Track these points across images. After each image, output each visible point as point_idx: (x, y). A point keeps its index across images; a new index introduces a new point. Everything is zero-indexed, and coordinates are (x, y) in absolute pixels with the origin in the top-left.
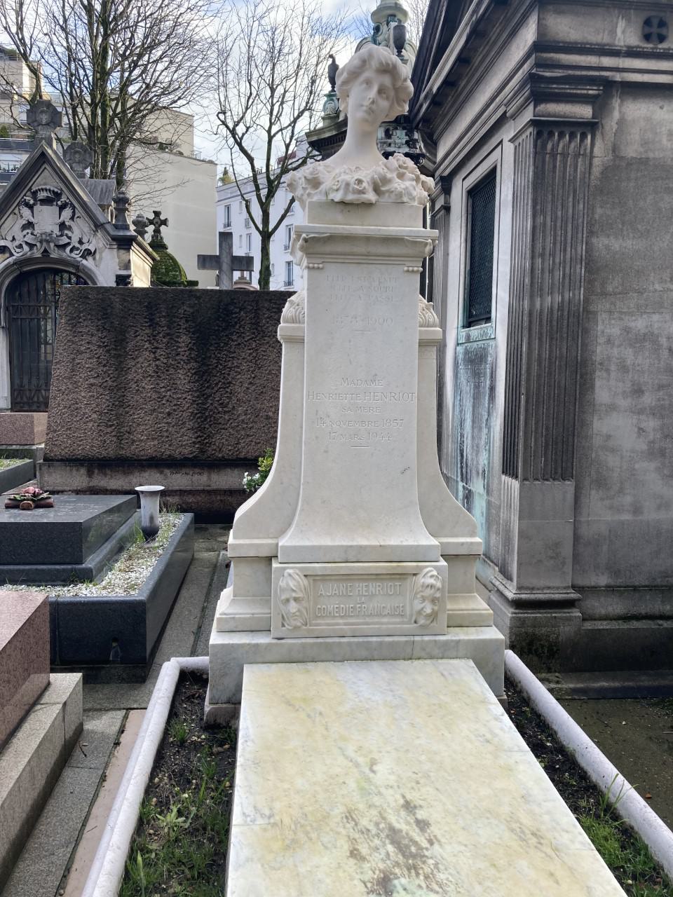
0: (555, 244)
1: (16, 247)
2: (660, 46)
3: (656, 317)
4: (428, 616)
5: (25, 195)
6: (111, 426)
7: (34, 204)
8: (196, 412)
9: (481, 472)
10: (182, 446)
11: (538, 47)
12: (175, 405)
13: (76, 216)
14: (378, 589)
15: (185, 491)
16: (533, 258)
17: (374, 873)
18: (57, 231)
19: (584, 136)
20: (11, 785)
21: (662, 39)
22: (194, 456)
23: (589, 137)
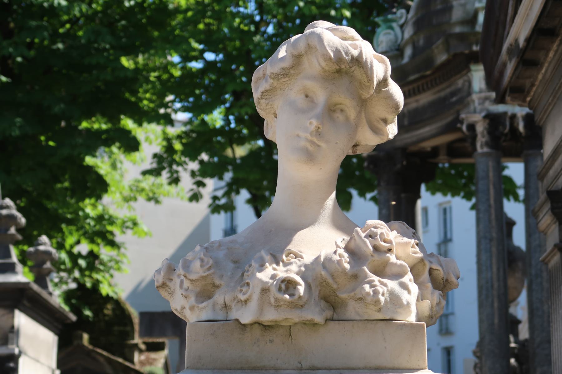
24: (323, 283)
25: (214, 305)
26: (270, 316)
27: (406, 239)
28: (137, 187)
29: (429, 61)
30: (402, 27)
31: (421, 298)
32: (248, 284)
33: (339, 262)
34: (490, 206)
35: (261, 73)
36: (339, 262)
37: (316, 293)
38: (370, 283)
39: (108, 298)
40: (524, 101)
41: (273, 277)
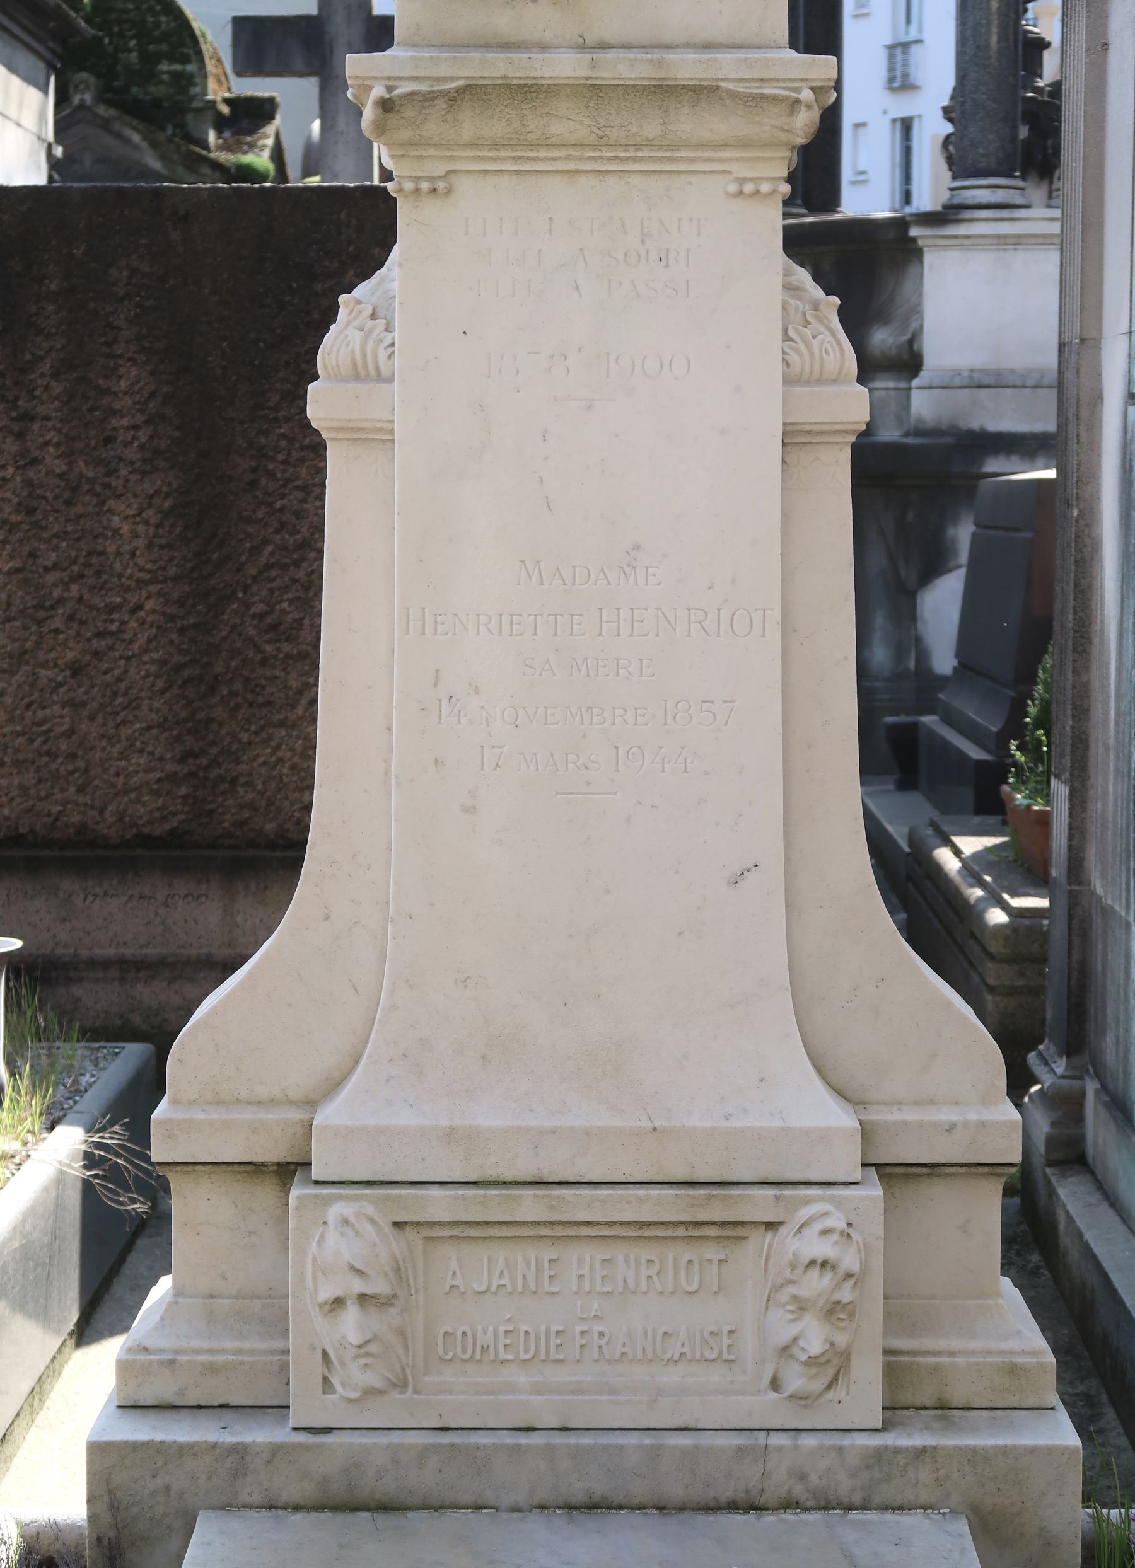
4: (812, 1362)
8: (177, 659)
10: (125, 791)
12: (99, 635)
14: (644, 1272)
22: (172, 832)
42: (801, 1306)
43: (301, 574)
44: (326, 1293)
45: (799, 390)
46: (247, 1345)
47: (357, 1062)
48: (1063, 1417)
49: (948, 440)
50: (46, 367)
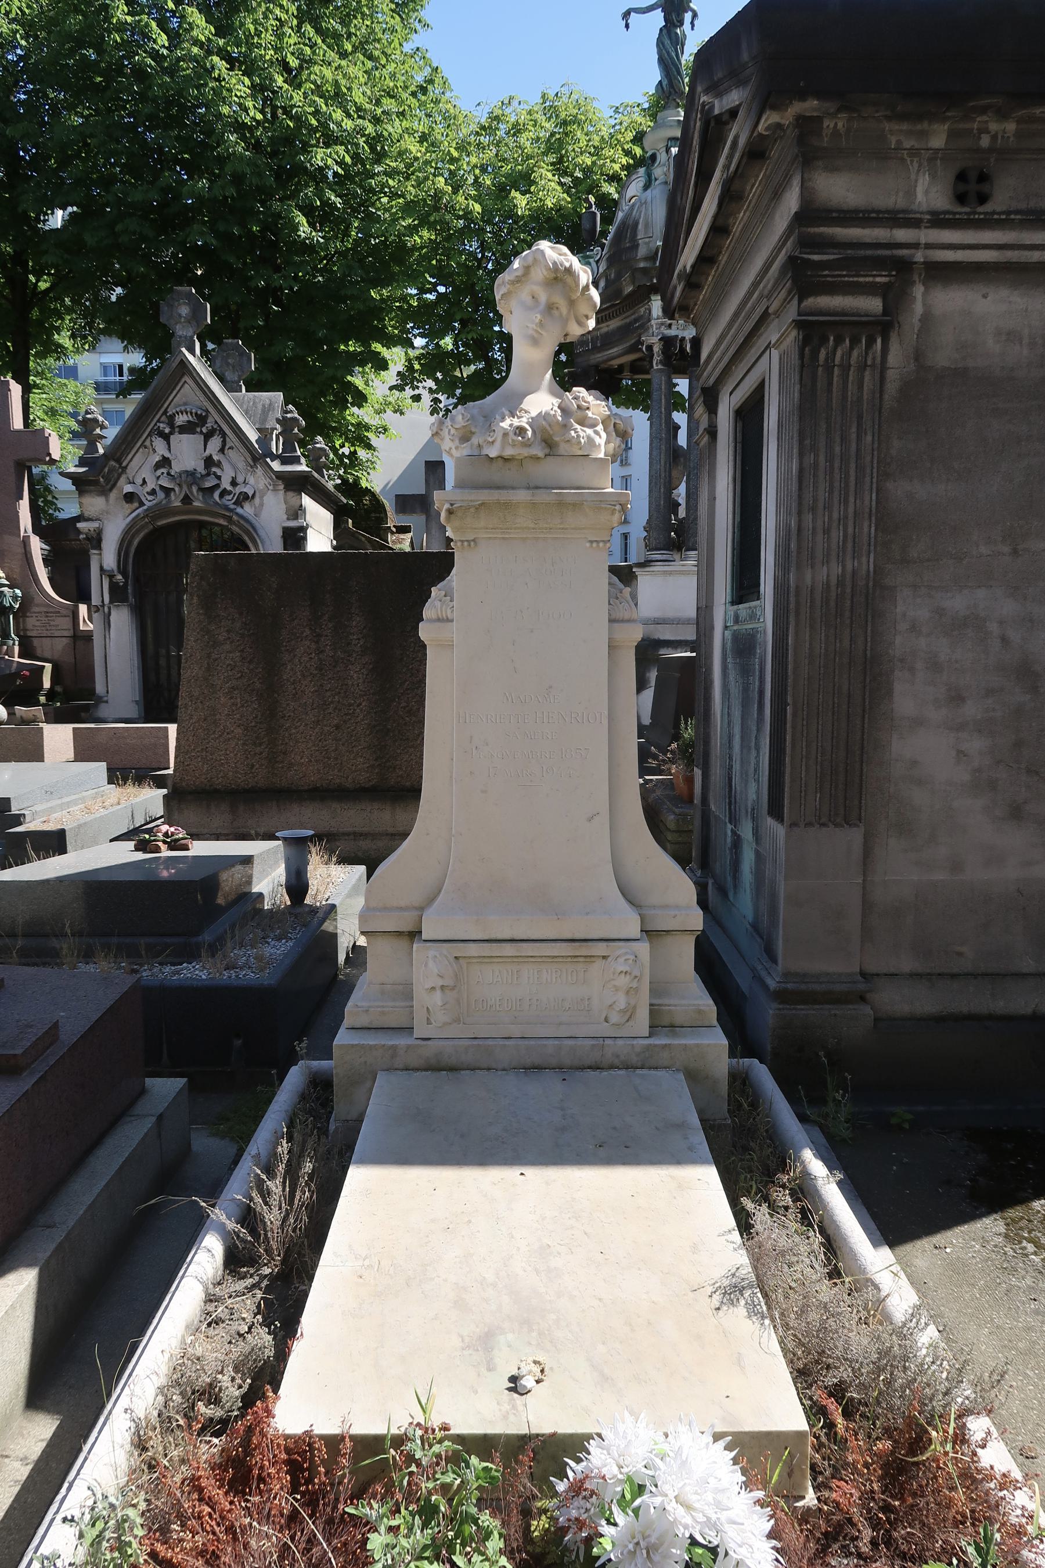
0: (831, 491)
1: (147, 493)
2: (980, 209)
3: (981, 593)
5: (159, 421)
6: (260, 744)
7: (171, 433)
9: (750, 810)
11: (802, 218)
13: (227, 447)
15: (361, 835)
16: (800, 513)
17: (477, 1327)
18: (201, 469)
19: (871, 342)
20: (81, 1212)
21: (983, 199)
23: (879, 341)
24: (543, 430)
25: (472, 445)
26: (509, 452)
27: (599, 402)
28: (386, 401)
29: (619, 292)
30: (597, 262)
31: (607, 442)
32: (494, 431)
33: (555, 415)
34: (661, 412)
35: (501, 280)
36: (555, 415)
37: (539, 436)
38: (575, 430)
39: (367, 491)
40: (689, 318)
41: (511, 425)
42: (617, 989)
43: (419, 692)
44: (428, 986)
45: (616, 625)
46: (397, 1004)
47: (440, 891)
48: (719, 1030)
49: (647, 643)
50: (326, 617)
